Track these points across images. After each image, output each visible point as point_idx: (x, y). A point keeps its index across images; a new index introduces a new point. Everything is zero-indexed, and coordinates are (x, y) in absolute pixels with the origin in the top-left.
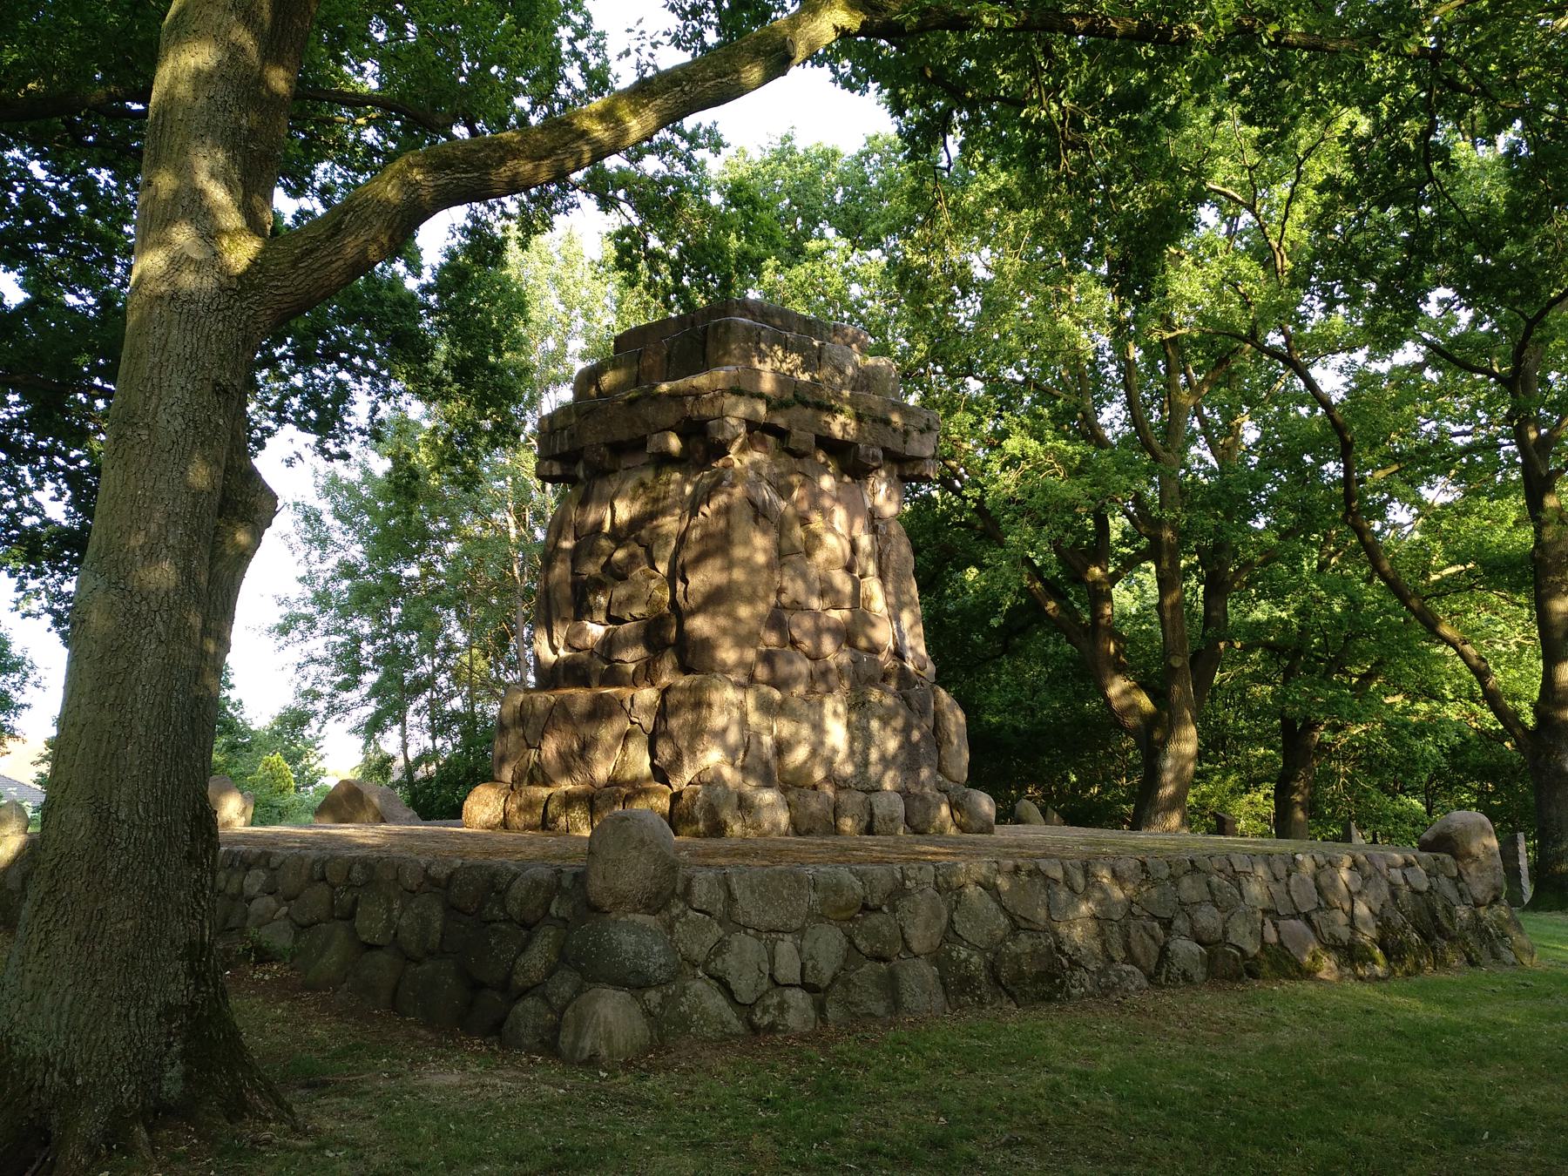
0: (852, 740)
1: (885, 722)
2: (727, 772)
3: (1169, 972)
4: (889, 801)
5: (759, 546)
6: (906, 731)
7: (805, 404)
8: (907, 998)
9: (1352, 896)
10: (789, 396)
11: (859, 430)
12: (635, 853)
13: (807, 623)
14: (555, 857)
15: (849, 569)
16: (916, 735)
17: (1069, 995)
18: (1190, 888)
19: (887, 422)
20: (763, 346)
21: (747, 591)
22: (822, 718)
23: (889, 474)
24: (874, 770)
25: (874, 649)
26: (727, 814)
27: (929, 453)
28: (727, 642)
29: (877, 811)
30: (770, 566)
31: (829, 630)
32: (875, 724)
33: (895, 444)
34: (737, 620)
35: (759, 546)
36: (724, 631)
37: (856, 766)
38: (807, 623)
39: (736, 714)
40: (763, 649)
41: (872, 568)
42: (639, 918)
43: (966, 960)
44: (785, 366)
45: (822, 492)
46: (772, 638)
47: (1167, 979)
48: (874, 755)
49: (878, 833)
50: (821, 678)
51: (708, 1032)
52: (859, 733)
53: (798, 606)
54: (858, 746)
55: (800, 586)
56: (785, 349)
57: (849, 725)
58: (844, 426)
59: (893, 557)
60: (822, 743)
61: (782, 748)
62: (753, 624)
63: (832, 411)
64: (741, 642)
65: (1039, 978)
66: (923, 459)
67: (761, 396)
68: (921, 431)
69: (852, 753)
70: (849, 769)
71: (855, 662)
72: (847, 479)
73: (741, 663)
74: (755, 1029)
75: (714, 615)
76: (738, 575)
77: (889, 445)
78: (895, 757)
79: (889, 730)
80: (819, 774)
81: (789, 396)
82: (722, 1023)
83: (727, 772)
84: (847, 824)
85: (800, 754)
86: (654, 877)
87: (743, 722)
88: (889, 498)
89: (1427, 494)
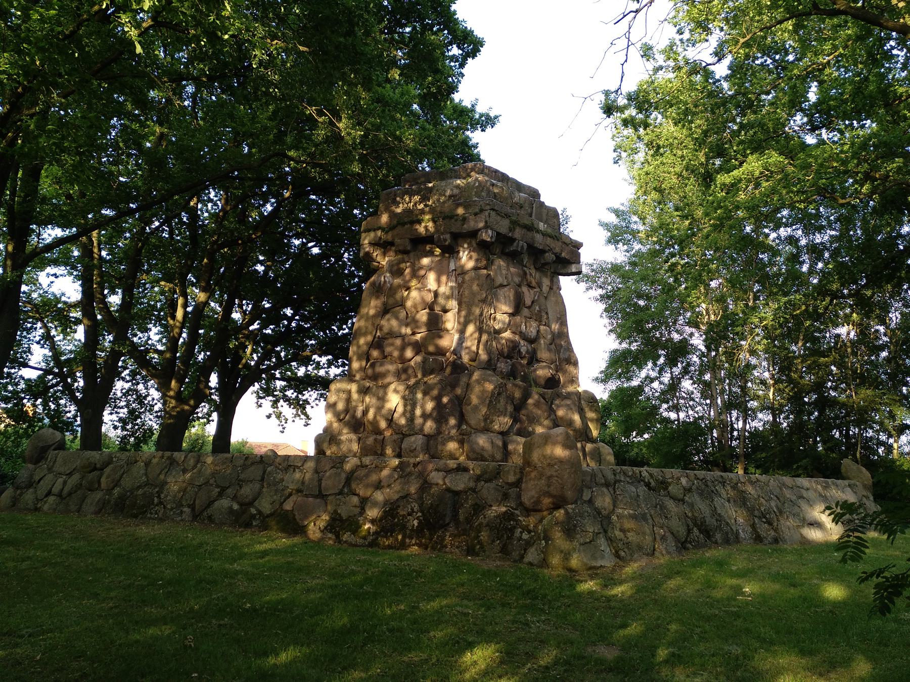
0: (405, 406)
1: (425, 393)
6: (438, 399)
7: (404, 224)
11: (436, 227)
13: (398, 342)
15: (431, 307)
16: (445, 400)
22: (386, 393)
23: (470, 245)
24: (419, 421)
25: (441, 352)
27: (481, 225)
30: (374, 316)
31: (410, 344)
32: (419, 396)
38: (398, 342)
39: (344, 396)
41: (453, 304)
45: (421, 268)
48: (418, 412)
52: (409, 401)
53: (392, 334)
54: (409, 408)
55: (394, 323)
58: (426, 227)
59: (466, 292)
60: (383, 407)
63: (419, 222)
66: (479, 230)
68: (476, 214)
70: (403, 421)
71: (424, 361)
72: (447, 255)
78: (431, 414)
79: (427, 398)
80: (383, 424)
87: (348, 400)
89: (855, 315)
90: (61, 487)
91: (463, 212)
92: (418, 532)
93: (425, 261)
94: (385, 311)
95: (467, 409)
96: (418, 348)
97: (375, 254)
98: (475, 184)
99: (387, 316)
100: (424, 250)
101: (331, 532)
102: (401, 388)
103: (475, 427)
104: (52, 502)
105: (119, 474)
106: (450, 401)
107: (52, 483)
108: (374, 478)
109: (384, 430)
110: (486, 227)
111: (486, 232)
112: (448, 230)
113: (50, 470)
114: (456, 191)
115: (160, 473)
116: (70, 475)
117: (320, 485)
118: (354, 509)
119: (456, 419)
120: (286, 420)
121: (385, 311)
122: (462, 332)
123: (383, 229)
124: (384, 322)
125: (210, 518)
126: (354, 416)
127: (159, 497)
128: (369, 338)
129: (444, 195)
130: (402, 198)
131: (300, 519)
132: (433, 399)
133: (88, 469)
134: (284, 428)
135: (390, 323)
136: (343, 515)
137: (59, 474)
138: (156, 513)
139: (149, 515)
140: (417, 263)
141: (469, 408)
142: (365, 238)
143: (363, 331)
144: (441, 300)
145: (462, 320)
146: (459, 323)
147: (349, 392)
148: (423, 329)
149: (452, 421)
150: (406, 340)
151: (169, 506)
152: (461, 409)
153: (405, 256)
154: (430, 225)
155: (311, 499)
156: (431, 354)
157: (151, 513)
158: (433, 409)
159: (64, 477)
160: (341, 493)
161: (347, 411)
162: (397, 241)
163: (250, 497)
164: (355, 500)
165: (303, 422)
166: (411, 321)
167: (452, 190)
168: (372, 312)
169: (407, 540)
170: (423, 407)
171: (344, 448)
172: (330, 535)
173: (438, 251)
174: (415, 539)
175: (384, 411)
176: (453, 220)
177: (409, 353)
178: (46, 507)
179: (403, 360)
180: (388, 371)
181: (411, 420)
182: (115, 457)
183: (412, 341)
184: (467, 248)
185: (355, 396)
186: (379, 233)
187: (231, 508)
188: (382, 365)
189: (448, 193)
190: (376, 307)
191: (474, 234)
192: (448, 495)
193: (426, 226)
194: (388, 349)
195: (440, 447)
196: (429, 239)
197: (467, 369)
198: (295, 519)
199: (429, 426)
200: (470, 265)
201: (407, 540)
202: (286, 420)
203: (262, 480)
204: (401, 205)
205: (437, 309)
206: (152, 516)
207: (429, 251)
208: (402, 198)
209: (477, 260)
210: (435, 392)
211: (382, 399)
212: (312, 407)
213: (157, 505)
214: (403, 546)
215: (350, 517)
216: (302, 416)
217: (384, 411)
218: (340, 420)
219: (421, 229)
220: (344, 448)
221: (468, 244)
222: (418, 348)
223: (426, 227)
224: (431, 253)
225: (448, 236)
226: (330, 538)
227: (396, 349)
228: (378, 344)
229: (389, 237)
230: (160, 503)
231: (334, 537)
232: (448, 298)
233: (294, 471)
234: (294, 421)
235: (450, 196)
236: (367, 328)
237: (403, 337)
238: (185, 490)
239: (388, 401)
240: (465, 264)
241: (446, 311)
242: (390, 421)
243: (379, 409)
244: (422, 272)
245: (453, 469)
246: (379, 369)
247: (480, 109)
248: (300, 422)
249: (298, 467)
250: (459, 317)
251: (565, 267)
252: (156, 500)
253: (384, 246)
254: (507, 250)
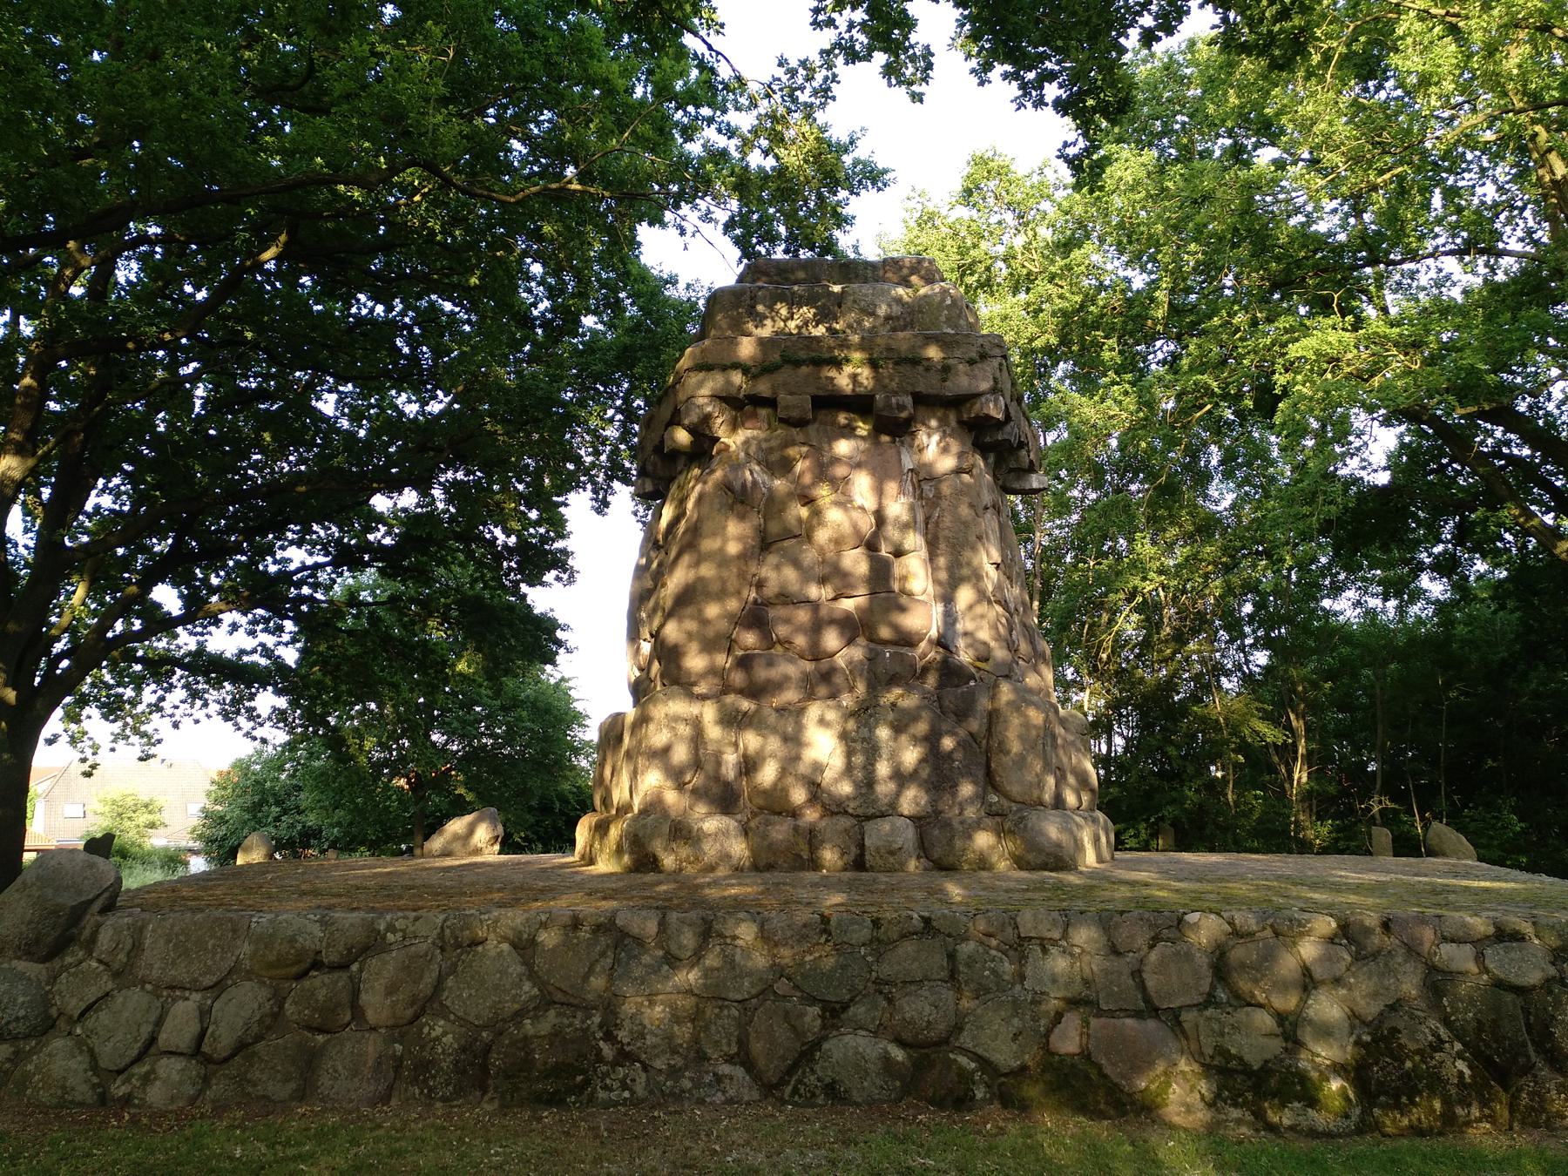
0: (849, 754)
1: (898, 729)
2: (671, 797)
3: (800, 1081)
4: (895, 833)
5: (734, 535)
6: (931, 741)
7: (797, 364)
8: (325, 1081)
9: (1308, 982)
10: (776, 357)
11: (877, 378)
12: (17, 896)
13: (803, 616)
14: (1278, 878)
15: (871, 546)
16: (948, 743)
17: (592, 1100)
18: (907, 958)
19: (916, 361)
20: (760, 308)
21: (715, 587)
22: (800, 727)
23: (943, 422)
24: (885, 788)
25: (907, 640)
26: (657, 846)
27: (985, 386)
28: (694, 647)
29: (867, 842)
30: (743, 557)
31: (832, 622)
32: (883, 733)
33: (927, 384)
34: (704, 622)
35: (734, 535)
36: (690, 636)
37: (856, 785)
38: (803, 616)
39: (685, 730)
40: (740, 653)
41: (914, 540)
42: (21, 965)
43: (438, 1039)
44: (792, 325)
45: (836, 460)
46: (750, 638)
47: (795, 1091)
48: (883, 769)
49: (872, 869)
50: (822, 681)
51: (44, 1096)
52: (860, 745)
53: (786, 598)
54: (858, 759)
55: (790, 574)
56: (791, 305)
57: (844, 736)
58: (854, 377)
59: (947, 521)
60: (797, 758)
61: (749, 765)
62: (723, 625)
63: (838, 364)
64: (709, 646)
65: (561, 1071)
66: (978, 395)
67: (736, 366)
68: (971, 362)
69: (849, 769)
70: (846, 788)
71: (872, 658)
72: (885, 438)
73: (712, 671)
74: (103, 1099)
75: (680, 620)
76: (707, 570)
77: (922, 388)
79: (904, 738)
80: (799, 795)
81: (776, 357)
82: (63, 1087)
83: (671, 797)
84: (829, 855)
85: (768, 774)
86: (30, 922)
87: (698, 738)
88: (945, 450)
90: (195, 1028)
91: (941, 355)
92: (1476, 1091)
93: (843, 447)
94: (764, 544)
95: (1000, 763)
96: (852, 628)
97: (719, 421)
98: (943, 300)
99: (772, 559)
100: (834, 423)
101: (1235, 1105)
102: (831, 715)
103: (1019, 798)
104: (176, 1077)
105: (429, 978)
106: (960, 744)
107: (153, 1017)
108: (1288, 965)
109: (801, 807)
110: (995, 390)
111: (996, 402)
112: (910, 388)
113: (123, 975)
114: (897, 310)
115: (591, 971)
116: (218, 988)
117: (1142, 986)
118: (1266, 1040)
119: (975, 783)
120: (96, 749)
121: (764, 544)
122: (948, 599)
123: (746, 370)
124: (767, 572)
125: (831, 1089)
126: (717, 778)
127: (609, 1037)
128: (733, 605)
129: (873, 314)
130: (771, 308)
131: (1123, 1077)
132: (916, 740)
133: (294, 970)
134: (94, 767)
135: (778, 575)
136: (1247, 1057)
137: (172, 988)
138: (624, 1087)
139: (602, 1095)
140: (826, 447)
141: (1005, 759)
142: (700, 384)
143: (715, 587)
144: (892, 532)
145: (943, 576)
146: (936, 581)
147: (697, 724)
148: (862, 590)
149: (967, 789)
150: (823, 612)
151: (659, 1064)
152: (988, 767)
153: (794, 431)
154: (865, 374)
155: (1129, 1021)
156: (885, 643)
157: (606, 1088)
158: (922, 761)
159: (196, 996)
160: (1210, 1001)
161: (697, 764)
162: (784, 398)
163: (942, 1026)
164: (1264, 1020)
165: (136, 751)
166: (833, 574)
167: (889, 306)
168: (733, 548)
169: (1459, 1111)
170: (894, 756)
171: (710, 850)
172: (1235, 1113)
173: (863, 429)
174: (1475, 1105)
175: (803, 768)
176: (921, 369)
177: (831, 640)
178: (156, 1095)
179: (816, 654)
180: (787, 678)
181: (868, 783)
182: (394, 931)
183: (837, 615)
184: (937, 429)
185: (714, 732)
186: (737, 378)
187: (886, 1059)
188: (770, 664)
189: (882, 310)
190: (740, 539)
191: (959, 402)
192: (1509, 997)
193: (851, 375)
194: (782, 631)
195: (958, 843)
196: (860, 404)
197: (972, 677)
198: (1105, 1076)
199: (911, 799)
200: (947, 463)
201: (1459, 1111)
202: (96, 749)
203: (953, 975)
204: (768, 322)
205: (884, 551)
206: (613, 1096)
207: (845, 426)
208: (771, 308)
209: (960, 456)
210: (922, 727)
211: (794, 740)
212: (197, 722)
213: (616, 1063)
214: (1449, 1121)
215: (1266, 1062)
216: (135, 739)
217: (803, 768)
218: (680, 787)
219: (843, 381)
220: (710, 850)
221: (940, 420)
222: (852, 628)
223: (854, 377)
224: (848, 432)
225: (908, 400)
226: (1239, 1122)
227: (799, 629)
228: (756, 617)
229: (763, 388)
230: (624, 1057)
231: (1249, 1117)
232: (905, 527)
233: (1045, 951)
234: (113, 750)
235: (888, 318)
236: (724, 582)
237: (815, 606)
238: (696, 1017)
239: (808, 745)
240: (935, 462)
241: (899, 553)
242: (816, 789)
243: (789, 764)
244: (840, 471)
245: (1487, 937)
246: (762, 674)
247: (861, 152)
248: (131, 750)
249: (1054, 942)
250: (935, 569)
251: (1019, 478)
252: (607, 1050)
253: (740, 406)
254: (988, 439)
